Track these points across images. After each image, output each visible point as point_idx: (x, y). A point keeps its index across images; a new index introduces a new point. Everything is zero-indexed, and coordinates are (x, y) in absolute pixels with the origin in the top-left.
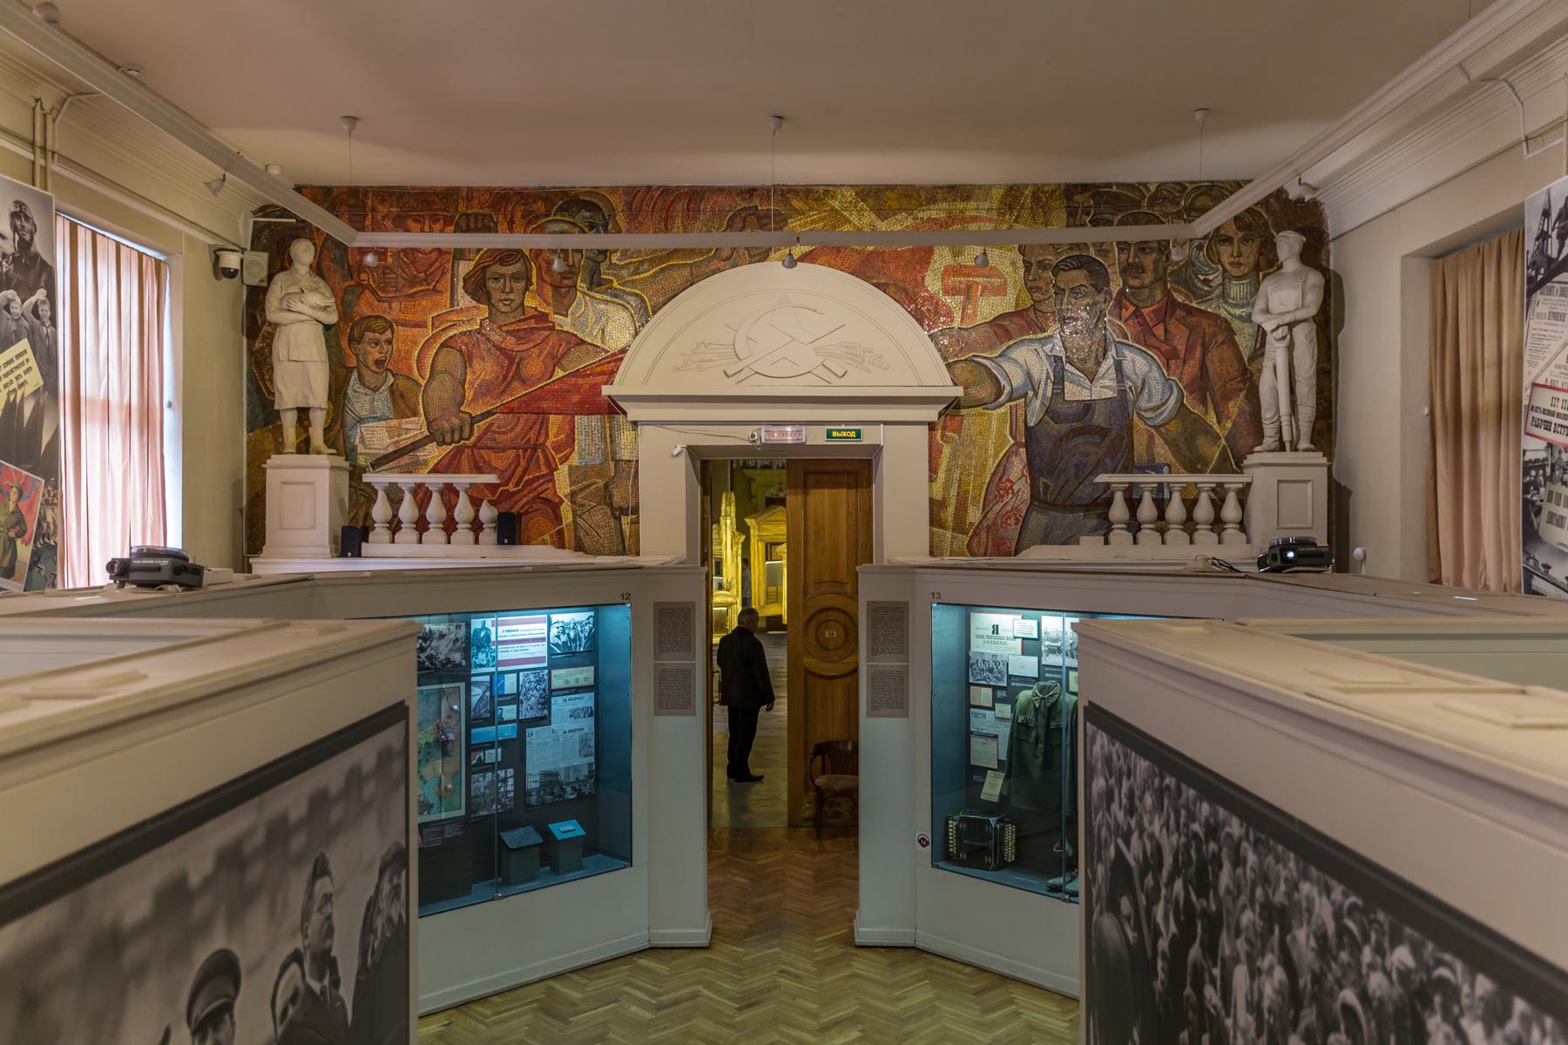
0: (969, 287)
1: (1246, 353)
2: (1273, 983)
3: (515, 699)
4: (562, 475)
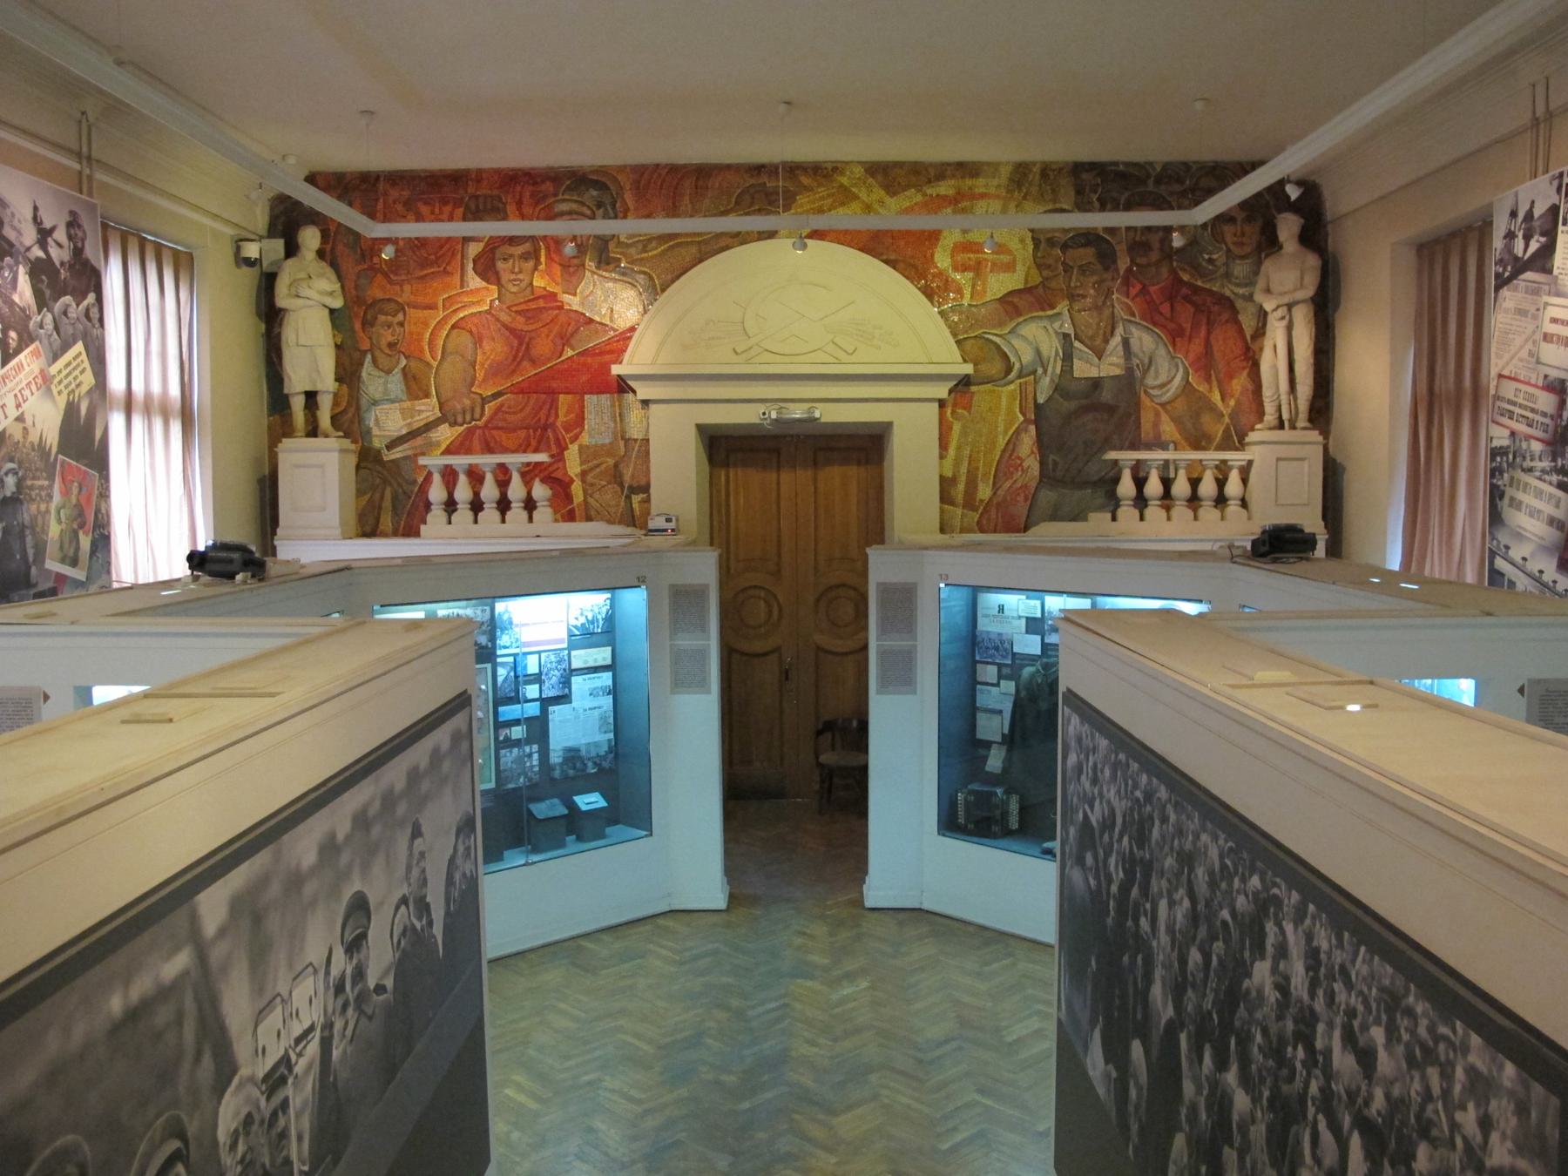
0: (979, 263)
1: (1248, 333)
2: (1180, 914)
3: (537, 679)
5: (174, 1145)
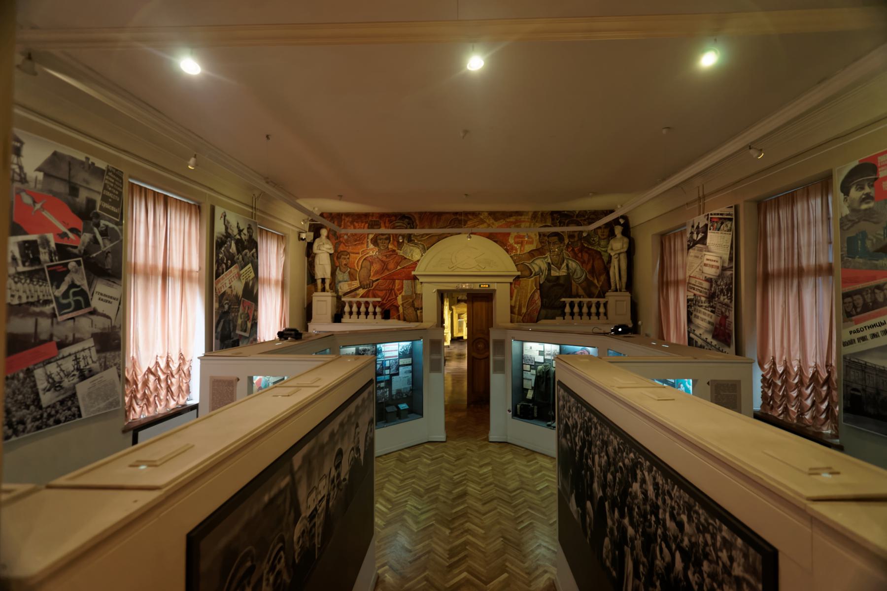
3: (389, 368)
4: (399, 298)
5: (280, 545)
